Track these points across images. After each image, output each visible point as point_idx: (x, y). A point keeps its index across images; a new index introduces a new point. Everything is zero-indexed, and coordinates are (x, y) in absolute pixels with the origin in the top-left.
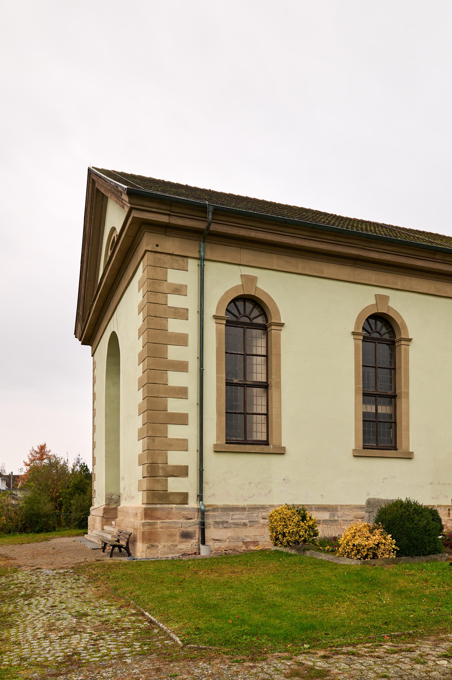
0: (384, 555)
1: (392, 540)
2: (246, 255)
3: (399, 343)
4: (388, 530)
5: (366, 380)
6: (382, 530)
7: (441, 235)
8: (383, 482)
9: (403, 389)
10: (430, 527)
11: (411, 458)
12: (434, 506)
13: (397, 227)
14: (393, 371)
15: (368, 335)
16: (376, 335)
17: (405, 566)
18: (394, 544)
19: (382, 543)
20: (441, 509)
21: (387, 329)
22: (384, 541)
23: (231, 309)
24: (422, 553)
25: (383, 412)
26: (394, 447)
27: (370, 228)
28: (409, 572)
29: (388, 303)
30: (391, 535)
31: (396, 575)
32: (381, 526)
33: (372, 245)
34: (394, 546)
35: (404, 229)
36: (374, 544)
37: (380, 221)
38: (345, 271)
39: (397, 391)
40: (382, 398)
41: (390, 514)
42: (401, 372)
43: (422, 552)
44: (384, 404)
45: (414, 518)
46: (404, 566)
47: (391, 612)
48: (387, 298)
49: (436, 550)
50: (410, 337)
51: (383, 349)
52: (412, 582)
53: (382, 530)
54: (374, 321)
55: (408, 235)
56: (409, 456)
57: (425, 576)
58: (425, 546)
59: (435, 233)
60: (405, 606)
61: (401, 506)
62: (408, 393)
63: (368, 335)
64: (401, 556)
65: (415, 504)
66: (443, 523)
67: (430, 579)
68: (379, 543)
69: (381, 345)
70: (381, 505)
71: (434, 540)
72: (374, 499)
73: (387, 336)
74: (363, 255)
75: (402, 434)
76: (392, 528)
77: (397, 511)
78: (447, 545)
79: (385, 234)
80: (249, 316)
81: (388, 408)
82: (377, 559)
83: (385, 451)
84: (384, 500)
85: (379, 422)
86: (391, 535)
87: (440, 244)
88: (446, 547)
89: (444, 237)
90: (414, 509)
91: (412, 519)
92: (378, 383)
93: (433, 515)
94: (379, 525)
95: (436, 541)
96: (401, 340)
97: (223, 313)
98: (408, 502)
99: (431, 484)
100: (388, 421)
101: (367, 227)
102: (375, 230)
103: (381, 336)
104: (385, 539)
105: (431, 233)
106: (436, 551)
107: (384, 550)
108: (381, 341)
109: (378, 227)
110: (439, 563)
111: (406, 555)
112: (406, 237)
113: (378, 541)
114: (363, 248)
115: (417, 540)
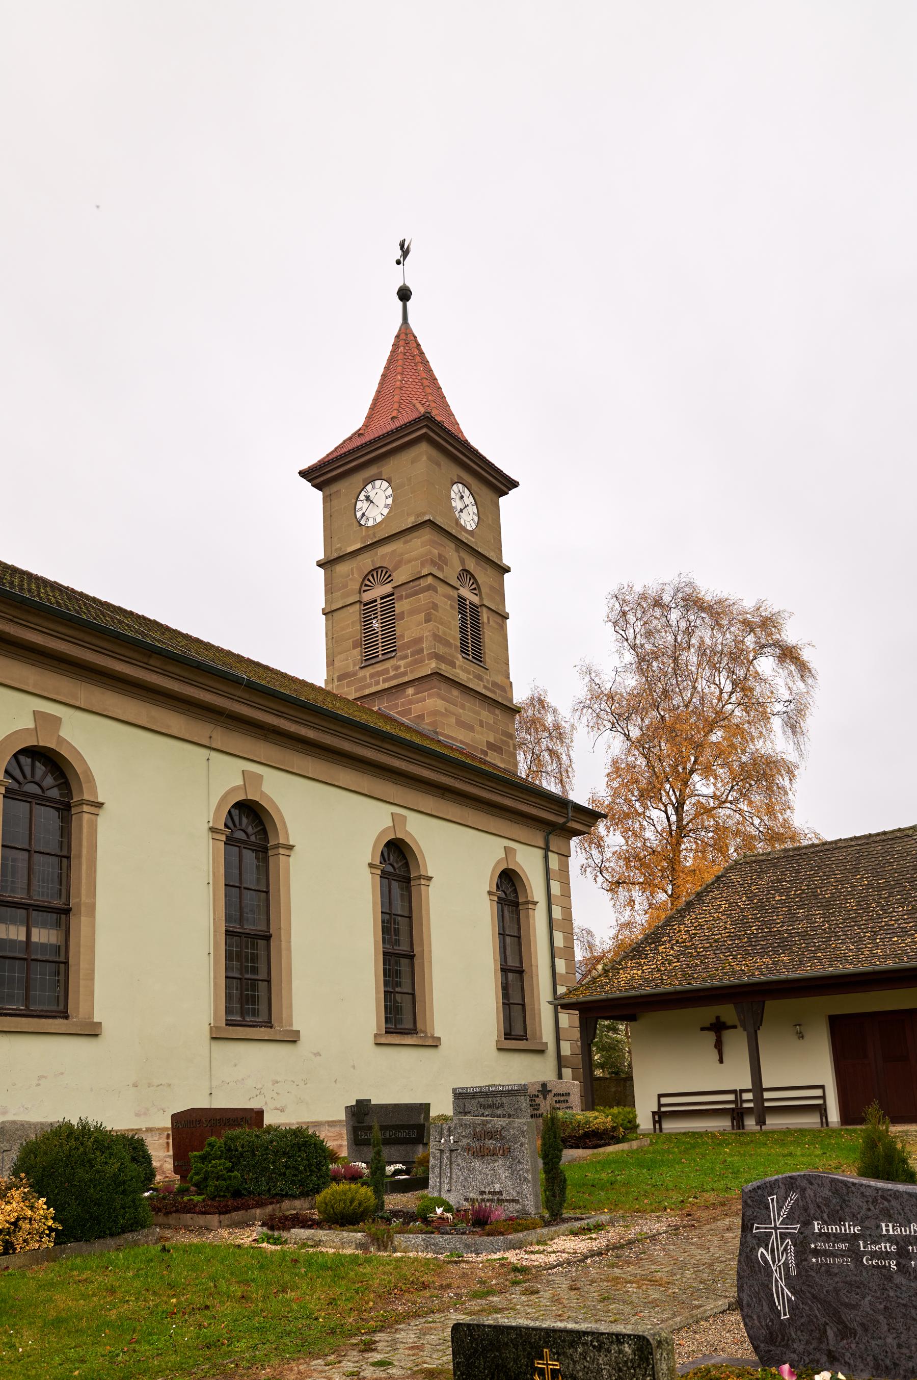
0: (28, 1244)
1: (48, 1209)
2: (264, 749)
3: (417, 882)
4: (39, 1189)
5: (9, 875)
6: (26, 1190)
7: (162, 625)
8: (38, 1085)
9: (83, 898)
10: (126, 1176)
11: (97, 1035)
12: (139, 1130)
13: (81, 594)
14: (65, 861)
15: (15, 786)
16: (32, 788)
17: (72, 1264)
18: (52, 1218)
19: (25, 1219)
20: (152, 1137)
21: (54, 779)
22: (29, 1213)
23: (11, 770)
24: (108, 1232)
25: (20, 939)
26: (63, 1012)
27: (29, 585)
28: (78, 1275)
29: (58, 729)
30: (45, 1200)
31: (52, 1285)
32: (24, 1181)
33: (30, 618)
34: (50, 1223)
35: (94, 600)
36: (7, 1222)
37: (51, 577)
38: (176, 722)
39: (73, 901)
40: (40, 913)
41: (46, 1153)
42: (80, 864)
43: (109, 1229)
44: (44, 925)
45: (94, 1159)
46: (69, 1263)
47: (34, 1372)
48: (57, 721)
49: (137, 1223)
50: (100, 800)
51: (47, 817)
52: (84, 1296)
53: (26, 1190)
54: (29, 760)
55: (103, 613)
56: (92, 1032)
57: (110, 1280)
58: (116, 1217)
59: (152, 618)
60: (64, 1353)
61: (68, 1136)
62: (94, 905)
63: (15, 786)
64: (64, 1243)
65: (98, 1129)
66: (155, 1164)
67: (120, 1287)
68: (18, 1219)
69: (43, 808)
70: (28, 1136)
71: (133, 1201)
72: (14, 1122)
73: (54, 793)
74: (12, 633)
75: (79, 987)
76: (49, 1184)
77: (61, 1146)
78: (160, 1210)
79: (57, 602)
80: (250, 832)
81: (53, 933)
82: (14, 1253)
83: (43, 1020)
84: (35, 1125)
85: (32, 960)
86: (45, 1200)
87: (159, 641)
88: (157, 1213)
89: (167, 629)
90: (96, 1141)
91: (89, 1161)
92: (35, 882)
93: (134, 1148)
94: (21, 1180)
95: (136, 1204)
96: (83, 804)
97: (494, 890)
98: (84, 1127)
99: (135, 1086)
100: (51, 959)
101: (22, 581)
102: (39, 591)
103: (43, 791)
104: (32, 1208)
105: (144, 618)
106: (136, 1225)
107: (29, 1233)
108: (43, 800)
109: (45, 587)
110: (140, 1250)
111: (77, 1240)
112: (98, 616)
113: (16, 1214)
114: (11, 621)
115: (99, 1205)
